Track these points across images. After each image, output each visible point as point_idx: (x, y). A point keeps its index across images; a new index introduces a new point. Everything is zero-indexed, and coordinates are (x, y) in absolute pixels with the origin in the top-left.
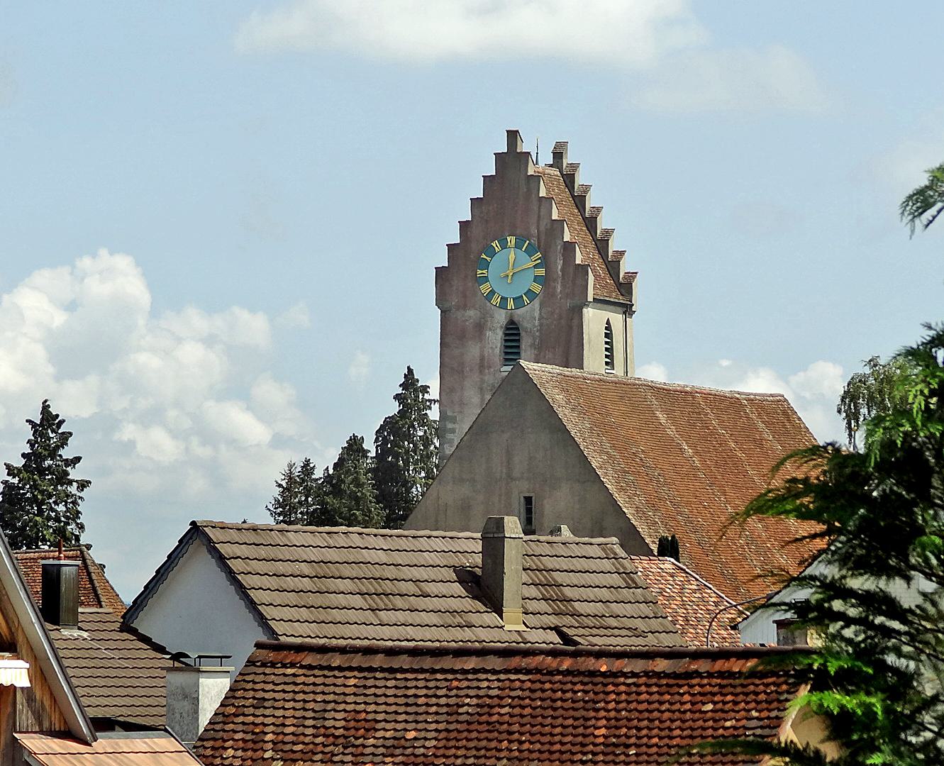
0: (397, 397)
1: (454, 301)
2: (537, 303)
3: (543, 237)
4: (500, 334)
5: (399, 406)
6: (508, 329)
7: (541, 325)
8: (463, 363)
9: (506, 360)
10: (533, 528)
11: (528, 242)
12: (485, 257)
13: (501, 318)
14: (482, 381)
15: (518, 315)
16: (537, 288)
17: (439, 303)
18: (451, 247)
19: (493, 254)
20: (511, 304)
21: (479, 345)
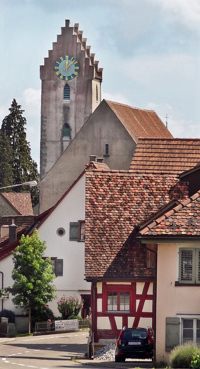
0: (10, 109)
1: (46, 77)
2: (76, 78)
3: (78, 55)
4: (63, 89)
6: (65, 87)
7: (77, 86)
9: (64, 97)
11: (73, 58)
12: (58, 63)
13: (63, 83)
14: (56, 104)
16: (76, 73)
17: (42, 76)
18: (45, 59)
19: (60, 61)
20: (67, 79)
21: (55, 92)
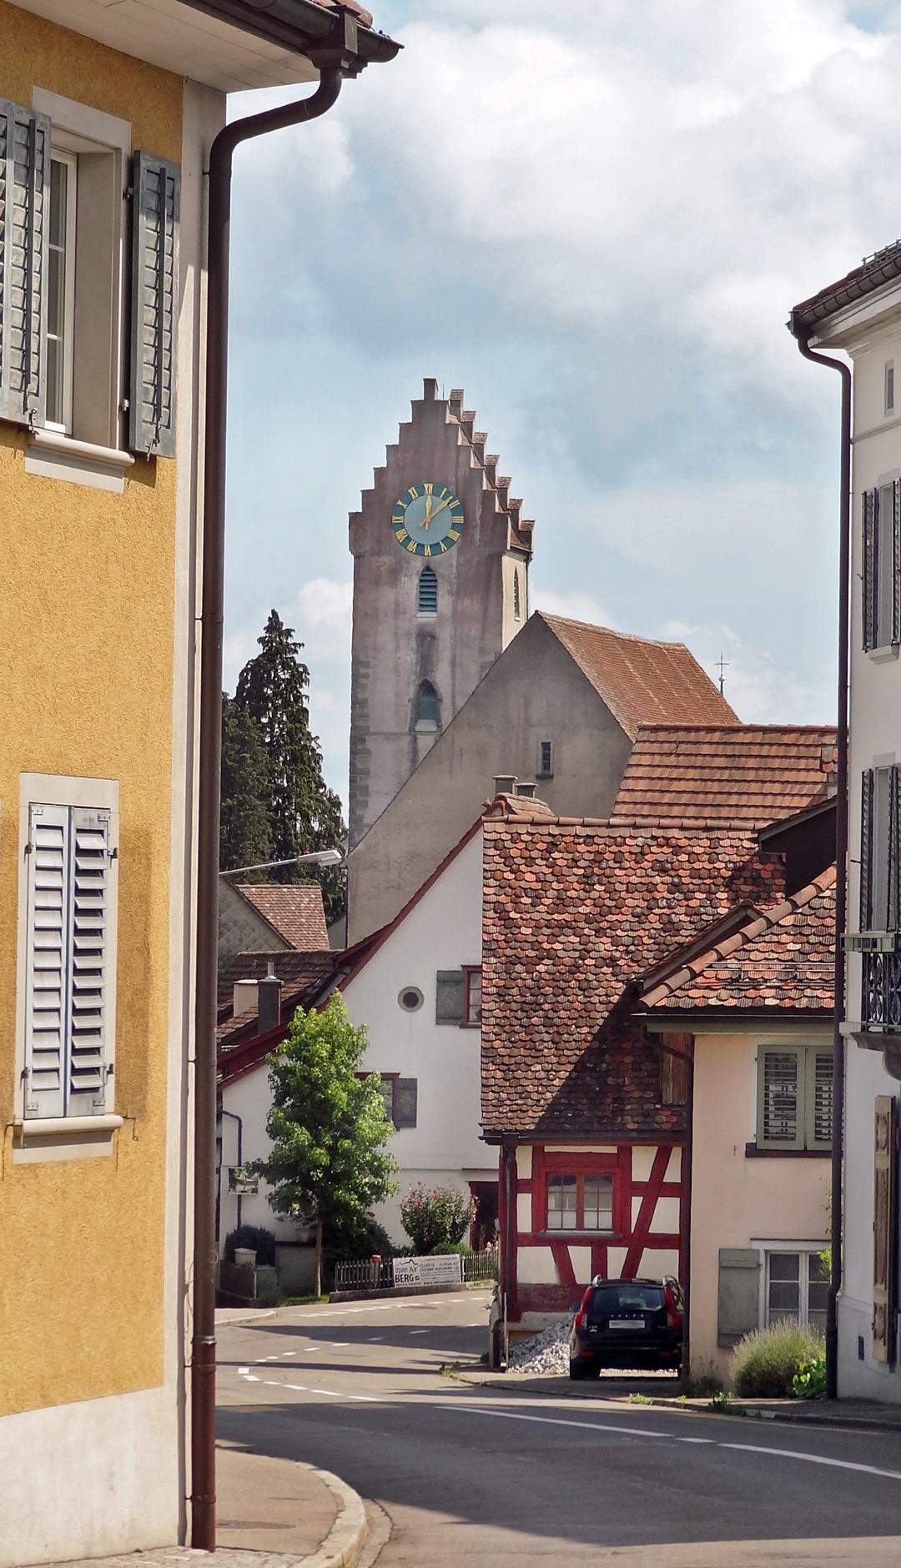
0: (261, 640)
2: (455, 548)
4: (416, 580)
5: (264, 649)
6: (423, 575)
7: (459, 572)
8: (378, 609)
9: (421, 605)
10: (551, 773)
11: (445, 489)
13: (418, 564)
15: (435, 562)
16: (455, 535)
18: (365, 493)
19: (409, 501)
20: (428, 551)
